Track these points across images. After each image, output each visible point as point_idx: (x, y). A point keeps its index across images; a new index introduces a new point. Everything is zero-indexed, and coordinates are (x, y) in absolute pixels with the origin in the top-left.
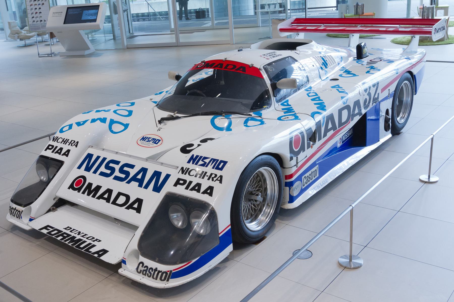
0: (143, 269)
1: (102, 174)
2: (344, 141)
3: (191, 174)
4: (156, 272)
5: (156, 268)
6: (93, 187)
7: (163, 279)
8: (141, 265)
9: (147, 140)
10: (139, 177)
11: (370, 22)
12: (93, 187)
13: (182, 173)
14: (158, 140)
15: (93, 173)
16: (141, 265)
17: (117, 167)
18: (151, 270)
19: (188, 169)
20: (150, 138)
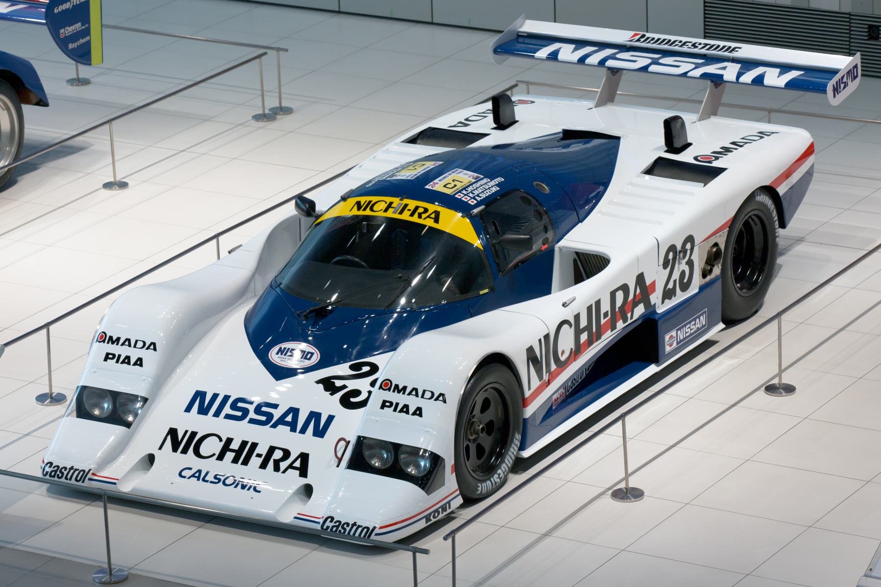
0: (331, 525)
1: (228, 417)
2: (681, 341)
3: (204, 450)
4: (355, 528)
13: (175, 449)
14: (309, 353)
19: (194, 434)
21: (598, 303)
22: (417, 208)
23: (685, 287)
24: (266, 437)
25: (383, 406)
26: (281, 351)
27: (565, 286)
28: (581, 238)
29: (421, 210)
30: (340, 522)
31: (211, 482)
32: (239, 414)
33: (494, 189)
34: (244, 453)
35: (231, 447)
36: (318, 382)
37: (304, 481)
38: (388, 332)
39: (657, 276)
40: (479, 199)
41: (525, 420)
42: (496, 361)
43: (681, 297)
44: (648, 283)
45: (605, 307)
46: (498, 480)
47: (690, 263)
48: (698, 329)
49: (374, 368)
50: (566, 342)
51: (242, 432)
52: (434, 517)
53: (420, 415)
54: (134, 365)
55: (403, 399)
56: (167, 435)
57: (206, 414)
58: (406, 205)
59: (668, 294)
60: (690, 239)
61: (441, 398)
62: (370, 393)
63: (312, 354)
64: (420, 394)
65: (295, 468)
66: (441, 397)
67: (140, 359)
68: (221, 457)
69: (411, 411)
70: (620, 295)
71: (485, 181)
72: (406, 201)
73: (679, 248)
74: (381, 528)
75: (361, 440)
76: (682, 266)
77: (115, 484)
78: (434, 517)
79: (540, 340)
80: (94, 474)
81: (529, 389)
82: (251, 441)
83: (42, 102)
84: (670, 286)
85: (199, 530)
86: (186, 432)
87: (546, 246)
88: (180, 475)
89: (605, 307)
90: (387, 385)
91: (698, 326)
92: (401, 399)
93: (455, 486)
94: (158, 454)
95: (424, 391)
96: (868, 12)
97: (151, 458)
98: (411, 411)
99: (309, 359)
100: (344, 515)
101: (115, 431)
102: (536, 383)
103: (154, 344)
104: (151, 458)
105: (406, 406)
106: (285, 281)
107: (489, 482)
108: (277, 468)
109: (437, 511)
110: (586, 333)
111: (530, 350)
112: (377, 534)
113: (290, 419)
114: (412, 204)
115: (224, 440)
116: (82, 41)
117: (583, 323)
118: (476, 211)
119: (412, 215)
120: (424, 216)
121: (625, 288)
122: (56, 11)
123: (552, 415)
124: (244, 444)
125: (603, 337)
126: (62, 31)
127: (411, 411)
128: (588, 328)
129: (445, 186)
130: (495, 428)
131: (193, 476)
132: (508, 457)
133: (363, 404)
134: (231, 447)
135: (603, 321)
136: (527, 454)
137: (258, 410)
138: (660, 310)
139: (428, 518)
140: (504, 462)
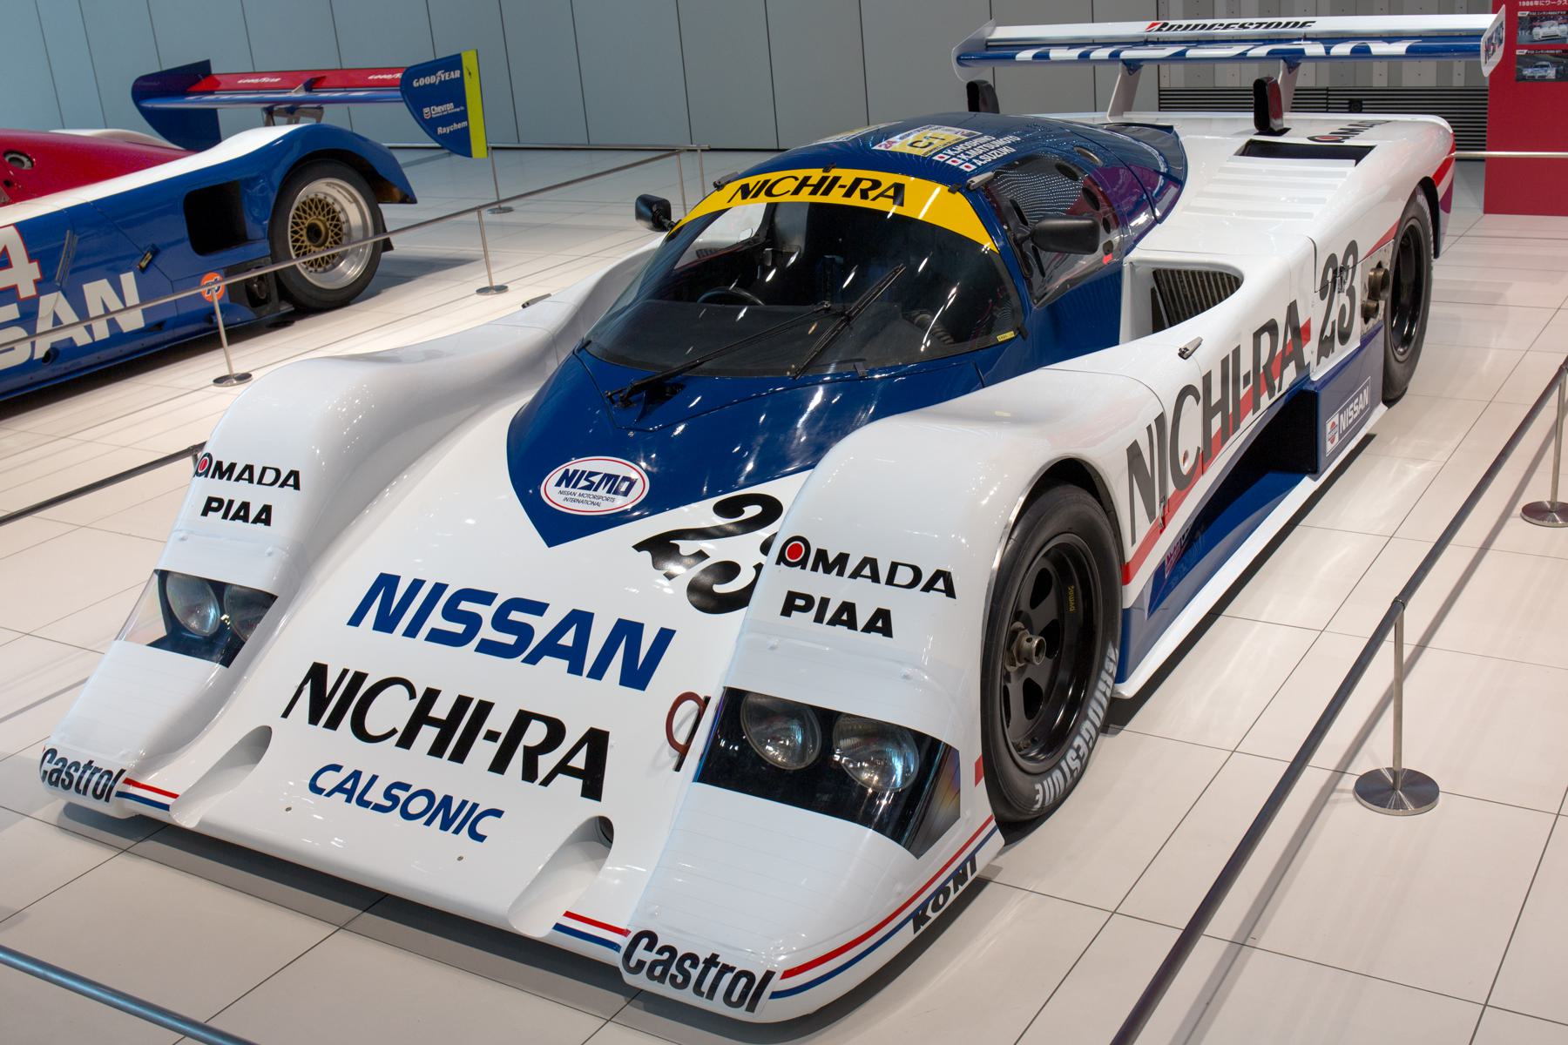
0: (649, 957)
1: (436, 636)
4: (713, 971)
5: (714, 956)
7: (735, 998)
8: (645, 941)
9: (583, 483)
10: (568, 639)
13: (314, 719)
14: (625, 479)
15: (405, 634)
16: (645, 941)
17: (487, 612)
18: (687, 964)
19: (359, 678)
20: (592, 474)
21: (1237, 352)
22: (858, 181)
23: (1344, 337)
24: (512, 687)
26: (567, 479)
27: (1139, 333)
28: (1169, 241)
29: (865, 185)
30: (672, 950)
31: (378, 808)
32: (515, 616)
33: (1006, 151)
34: (455, 730)
35: (432, 714)
37: (592, 809)
38: (810, 424)
39: (1312, 312)
41: (1127, 612)
42: (1069, 475)
43: (1341, 353)
44: (1302, 323)
45: (1246, 366)
46: (1076, 764)
47: (1351, 293)
48: (1362, 412)
49: (772, 509)
50: (1190, 440)
51: (459, 673)
52: (936, 908)
53: (887, 631)
54: (255, 521)
55: (841, 589)
56: (305, 682)
57: (391, 631)
58: (836, 179)
59: (1325, 346)
61: (940, 584)
62: (759, 568)
63: (632, 483)
64: (883, 574)
65: (574, 772)
66: (943, 582)
67: (267, 509)
68: (406, 741)
69: (862, 621)
71: (986, 138)
72: (834, 172)
74: (788, 974)
75: (734, 698)
76: (1342, 299)
77: (166, 807)
78: (934, 910)
79: (1149, 428)
80: (128, 782)
81: (1134, 542)
82: (477, 696)
83: (408, 198)
84: (1328, 333)
85: (342, 936)
86: (345, 672)
88: (314, 788)
89: (1246, 366)
90: (796, 553)
91: (1362, 406)
92: (836, 589)
93: (986, 810)
94: (280, 727)
95: (894, 567)
96: (1350, 84)
97: (261, 739)
98: (863, 618)
99: (626, 493)
100: (688, 934)
101: (205, 670)
103: (294, 474)
104: (261, 739)
105: (848, 608)
106: (605, 341)
107: (1057, 774)
108: (529, 773)
109: (943, 890)
111: (1134, 452)
112: (775, 995)
113: (570, 643)
114: (847, 176)
115: (420, 694)
116: (456, 126)
117: (1216, 396)
118: (977, 180)
119: (848, 194)
120: (872, 194)
121: (1271, 327)
122: (415, 84)
123: (1169, 589)
124: (462, 703)
125: (1243, 425)
126: (426, 110)
127: (862, 621)
129: (911, 145)
130: (1065, 622)
131: (339, 788)
132: (1094, 704)
133: (740, 600)
134: (432, 714)
135: (1243, 392)
136: (1129, 689)
137: (500, 622)
139: (918, 918)
140: (1086, 717)
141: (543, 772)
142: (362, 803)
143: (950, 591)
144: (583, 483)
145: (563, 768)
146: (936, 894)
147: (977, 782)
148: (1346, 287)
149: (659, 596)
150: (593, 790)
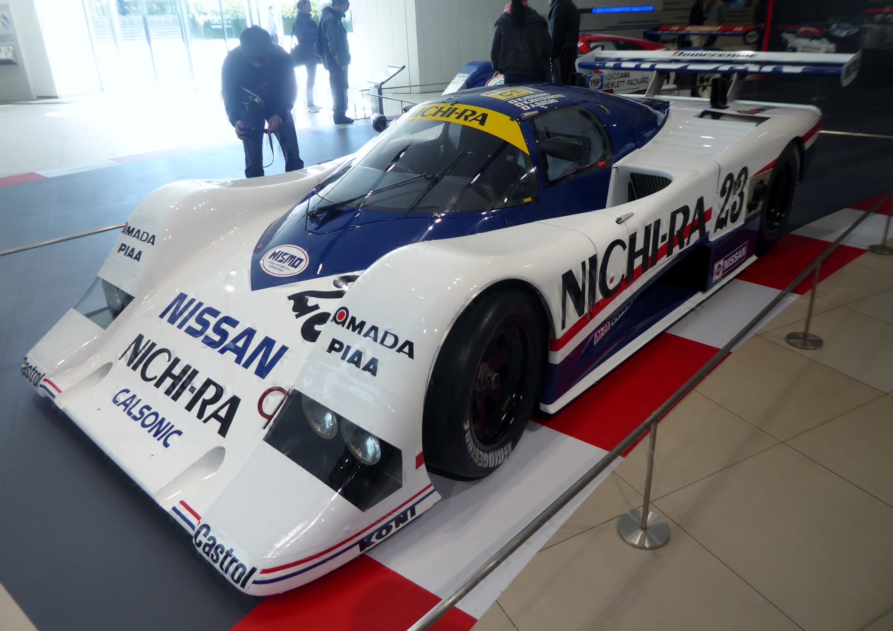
4: (229, 559)
5: (232, 550)
6: (357, 323)
10: (240, 344)
11: (612, 348)
12: (357, 323)
14: (299, 259)
16: (204, 530)
20: (286, 254)
21: (658, 223)
22: (466, 111)
23: (734, 218)
25: (331, 348)
27: (617, 203)
28: (640, 160)
33: (552, 101)
34: (178, 380)
35: (173, 372)
36: (290, 298)
39: (714, 203)
40: (533, 106)
43: (730, 227)
44: (706, 208)
45: (664, 230)
47: (741, 195)
48: (740, 259)
50: (617, 267)
53: (374, 372)
59: (721, 223)
60: (745, 170)
63: (301, 260)
64: (380, 336)
66: (408, 348)
70: (680, 217)
73: (735, 178)
74: (264, 571)
76: (734, 198)
78: (377, 538)
79: (583, 264)
80: (46, 380)
81: (563, 327)
84: (723, 216)
87: (604, 163)
88: (115, 401)
89: (664, 230)
91: (740, 256)
92: (355, 341)
97: (108, 367)
98: (365, 361)
102: (573, 318)
104: (108, 367)
105: (359, 354)
110: (641, 257)
111: (568, 278)
112: (255, 582)
117: (639, 246)
121: (685, 210)
124: (188, 367)
125: (659, 263)
128: (644, 251)
131: (124, 403)
135: (660, 245)
138: (713, 238)
141: (206, 416)
142: (129, 413)
143: (411, 354)
144: (280, 258)
145: (215, 415)
146: (381, 529)
147: (417, 466)
148: (738, 192)
149: (284, 326)
150: (223, 432)
